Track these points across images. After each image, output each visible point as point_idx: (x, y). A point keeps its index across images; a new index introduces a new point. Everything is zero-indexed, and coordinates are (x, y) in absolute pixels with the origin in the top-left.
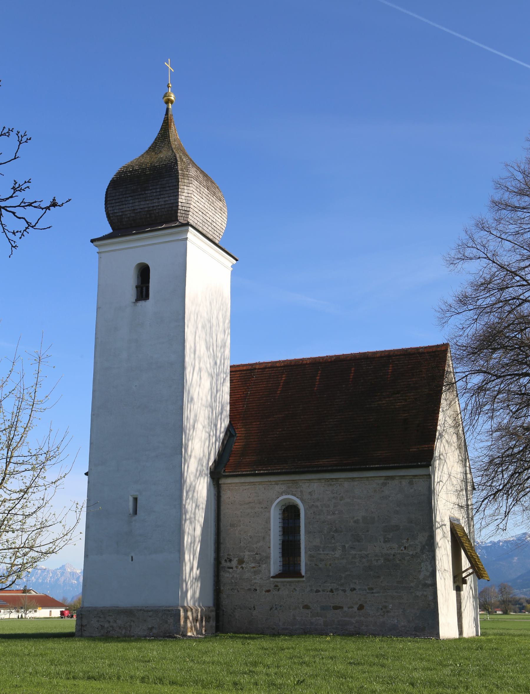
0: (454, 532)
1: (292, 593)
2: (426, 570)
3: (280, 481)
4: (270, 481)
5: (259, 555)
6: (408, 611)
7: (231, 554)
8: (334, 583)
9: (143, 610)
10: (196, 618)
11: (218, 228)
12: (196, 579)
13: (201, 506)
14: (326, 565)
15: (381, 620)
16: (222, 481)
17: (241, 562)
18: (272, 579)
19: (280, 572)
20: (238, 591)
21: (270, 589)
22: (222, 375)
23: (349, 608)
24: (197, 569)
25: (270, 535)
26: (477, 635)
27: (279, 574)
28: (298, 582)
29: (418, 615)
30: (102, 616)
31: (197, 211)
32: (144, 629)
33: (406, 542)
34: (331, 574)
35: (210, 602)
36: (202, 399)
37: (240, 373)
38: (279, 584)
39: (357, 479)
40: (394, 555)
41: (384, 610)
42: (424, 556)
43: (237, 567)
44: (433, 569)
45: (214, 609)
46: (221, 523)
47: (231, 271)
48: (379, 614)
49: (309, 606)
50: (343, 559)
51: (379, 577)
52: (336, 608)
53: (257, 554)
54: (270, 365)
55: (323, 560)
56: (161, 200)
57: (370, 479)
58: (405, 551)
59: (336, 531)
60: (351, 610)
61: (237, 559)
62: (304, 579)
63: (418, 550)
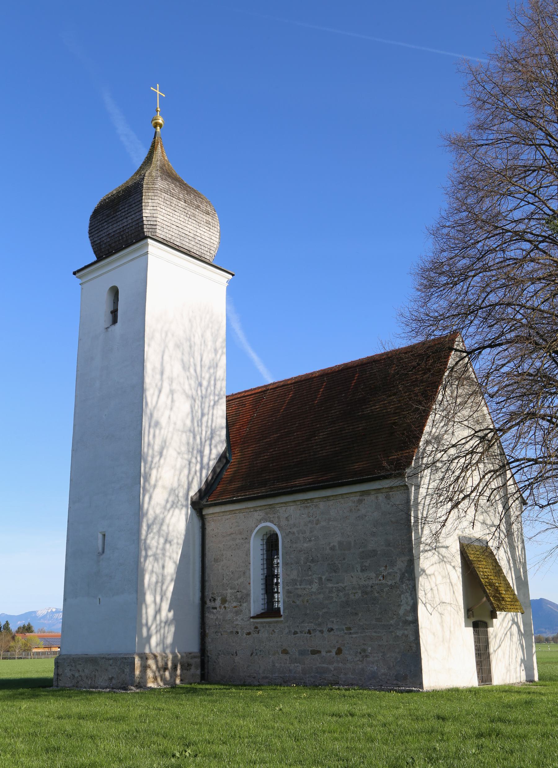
0: (465, 555)
1: (271, 635)
2: (407, 603)
3: (257, 507)
4: (248, 508)
5: (240, 593)
6: (388, 656)
7: (215, 592)
8: (312, 622)
9: (106, 658)
10: (165, 666)
11: (208, 243)
12: (166, 623)
13: (175, 541)
14: (303, 602)
15: (360, 667)
16: (205, 512)
17: (224, 601)
18: (252, 620)
19: (263, 611)
20: (222, 634)
21: (251, 631)
22: (212, 397)
23: (326, 652)
24: (169, 610)
25: (249, 569)
26: (530, 680)
27: (261, 613)
28: (277, 622)
29: (399, 660)
30: (73, 665)
31: (169, 224)
32: (105, 680)
33: (384, 570)
34: (308, 612)
35: (195, 648)
36: (175, 424)
37: (255, 396)
38: (259, 626)
39: (332, 498)
40: (372, 587)
41: (363, 654)
42: (404, 586)
43: (220, 607)
44: (414, 602)
45: (199, 654)
46: (206, 559)
47: (227, 287)
48: (358, 659)
49: (288, 651)
50: (320, 593)
51: (357, 614)
52: (314, 652)
53: (238, 592)
54: (282, 383)
55: (301, 596)
56: (129, 218)
57: (345, 496)
58: (384, 582)
59: (313, 561)
60: (329, 654)
61: (221, 597)
62: (282, 619)
63: (398, 579)
